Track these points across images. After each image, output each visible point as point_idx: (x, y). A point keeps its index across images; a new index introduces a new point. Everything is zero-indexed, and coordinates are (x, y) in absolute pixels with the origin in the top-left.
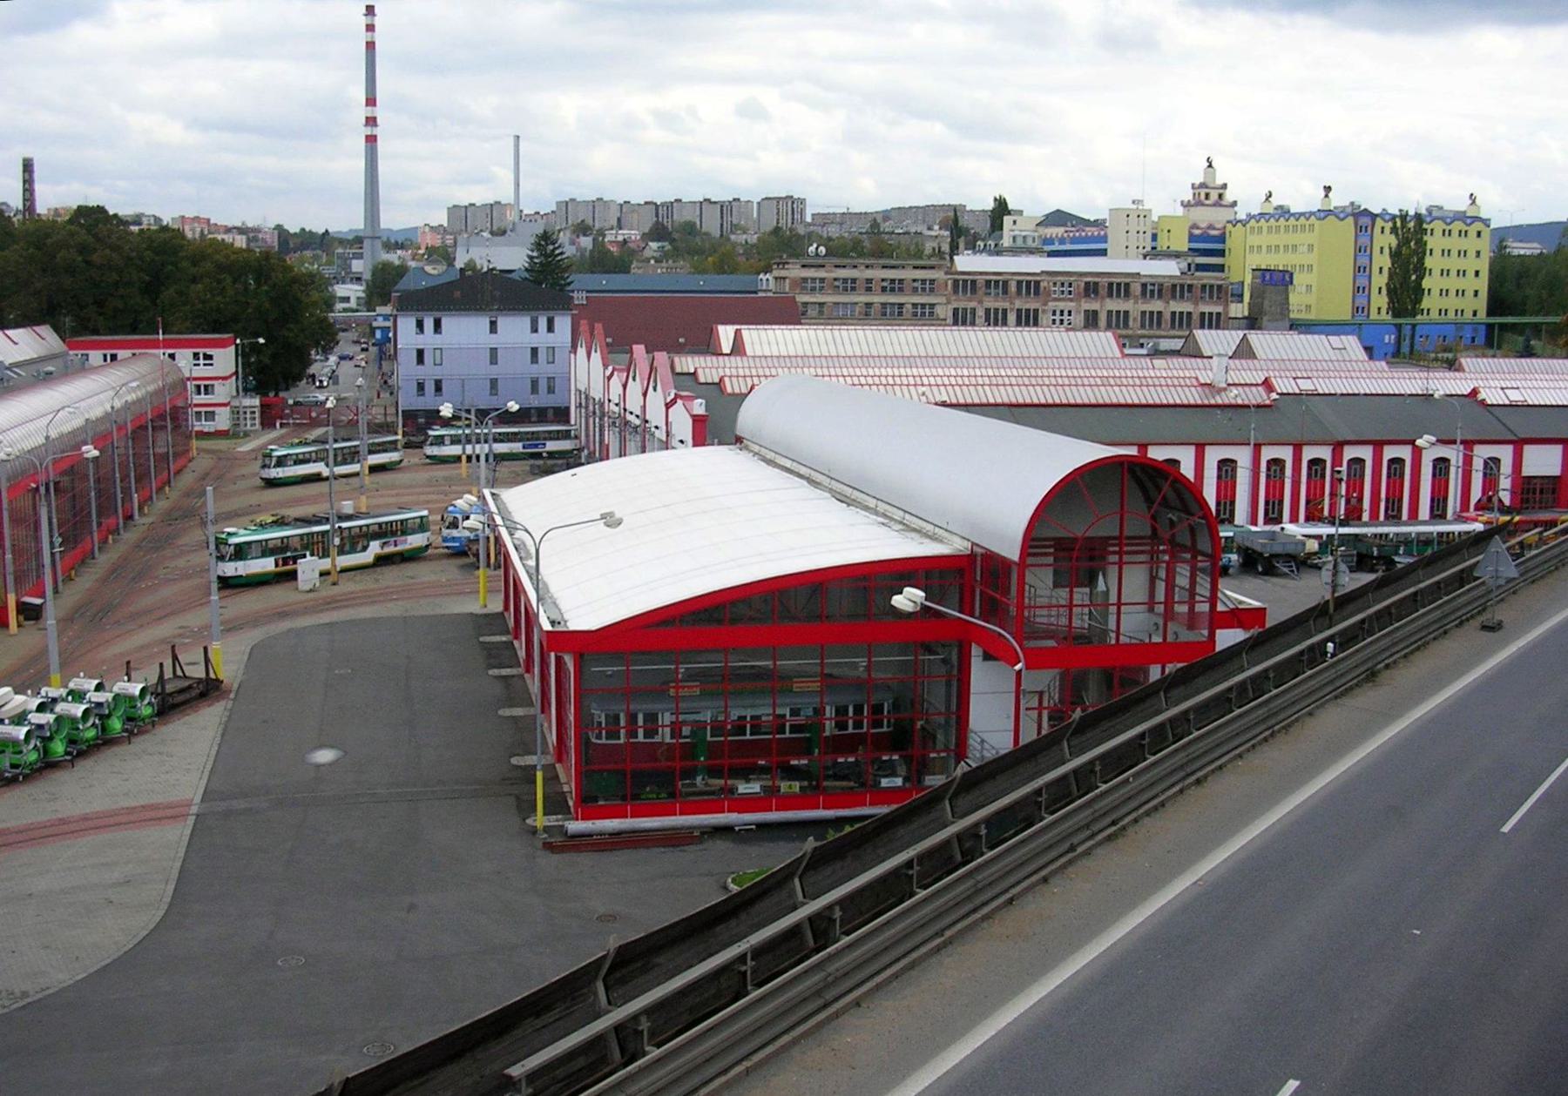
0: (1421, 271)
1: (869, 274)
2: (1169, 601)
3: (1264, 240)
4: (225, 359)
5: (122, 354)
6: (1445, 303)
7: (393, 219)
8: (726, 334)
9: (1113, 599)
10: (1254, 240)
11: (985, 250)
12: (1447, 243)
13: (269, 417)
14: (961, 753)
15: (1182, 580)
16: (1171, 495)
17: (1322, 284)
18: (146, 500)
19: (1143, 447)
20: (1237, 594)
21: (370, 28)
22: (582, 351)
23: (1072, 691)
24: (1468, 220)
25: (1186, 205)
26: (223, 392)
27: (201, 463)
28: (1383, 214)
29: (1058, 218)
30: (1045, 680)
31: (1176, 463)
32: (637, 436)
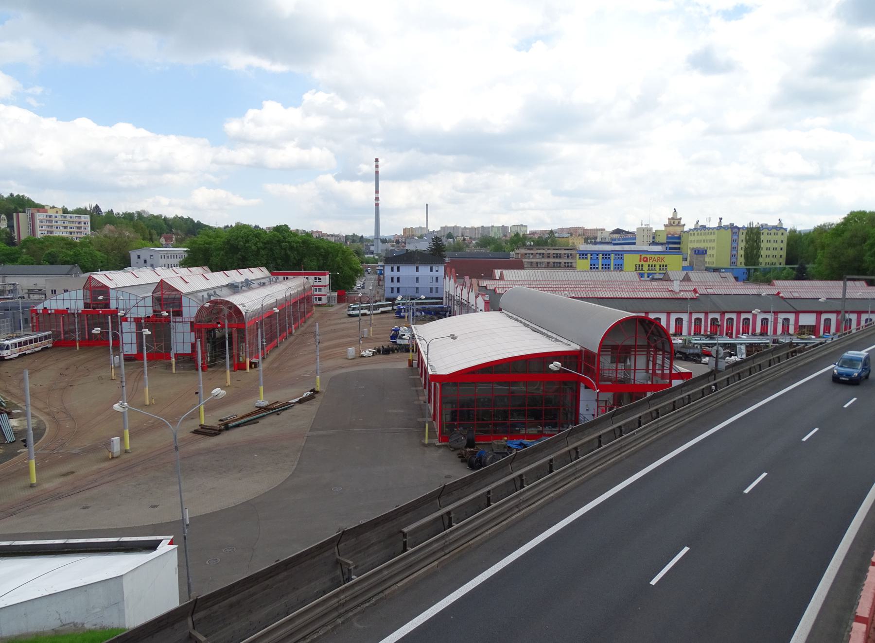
0: (759, 248)
1: (549, 252)
2: (654, 370)
3: (696, 238)
4: (326, 279)
5: (289, 277)
6: (768, 260)
7: (384, 233)
8: (497, 273)
9: (633, 368)
10: (691, 238)
11: (591, 243)
12: (769, 237)
13: (341, 299)
14: (577, 421)
15: (659, 362)
16: (655, 331)
17: (718, 254)
18: (296, 328)
19: (647, 313)
20: (682, 367)
21: (377, 166)
22: (447, 278)
23: (618, 401)
24: (778, 228)
25: (666, 226)
26: (325, 291)
27: (316, 315)
28: (743, 228)
29: (618, 231)
30: (608, 396)
31: (660, 319)
32: (466, 308)
